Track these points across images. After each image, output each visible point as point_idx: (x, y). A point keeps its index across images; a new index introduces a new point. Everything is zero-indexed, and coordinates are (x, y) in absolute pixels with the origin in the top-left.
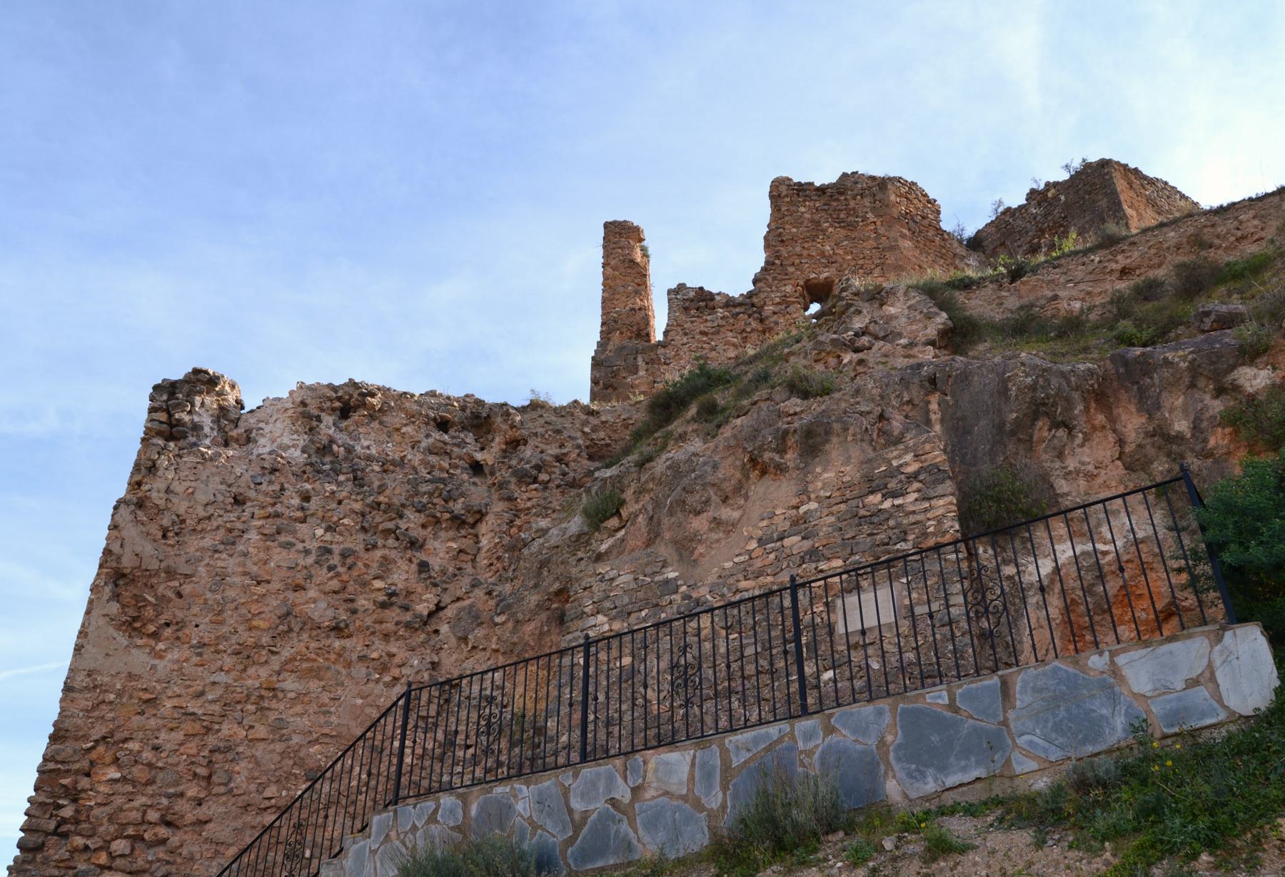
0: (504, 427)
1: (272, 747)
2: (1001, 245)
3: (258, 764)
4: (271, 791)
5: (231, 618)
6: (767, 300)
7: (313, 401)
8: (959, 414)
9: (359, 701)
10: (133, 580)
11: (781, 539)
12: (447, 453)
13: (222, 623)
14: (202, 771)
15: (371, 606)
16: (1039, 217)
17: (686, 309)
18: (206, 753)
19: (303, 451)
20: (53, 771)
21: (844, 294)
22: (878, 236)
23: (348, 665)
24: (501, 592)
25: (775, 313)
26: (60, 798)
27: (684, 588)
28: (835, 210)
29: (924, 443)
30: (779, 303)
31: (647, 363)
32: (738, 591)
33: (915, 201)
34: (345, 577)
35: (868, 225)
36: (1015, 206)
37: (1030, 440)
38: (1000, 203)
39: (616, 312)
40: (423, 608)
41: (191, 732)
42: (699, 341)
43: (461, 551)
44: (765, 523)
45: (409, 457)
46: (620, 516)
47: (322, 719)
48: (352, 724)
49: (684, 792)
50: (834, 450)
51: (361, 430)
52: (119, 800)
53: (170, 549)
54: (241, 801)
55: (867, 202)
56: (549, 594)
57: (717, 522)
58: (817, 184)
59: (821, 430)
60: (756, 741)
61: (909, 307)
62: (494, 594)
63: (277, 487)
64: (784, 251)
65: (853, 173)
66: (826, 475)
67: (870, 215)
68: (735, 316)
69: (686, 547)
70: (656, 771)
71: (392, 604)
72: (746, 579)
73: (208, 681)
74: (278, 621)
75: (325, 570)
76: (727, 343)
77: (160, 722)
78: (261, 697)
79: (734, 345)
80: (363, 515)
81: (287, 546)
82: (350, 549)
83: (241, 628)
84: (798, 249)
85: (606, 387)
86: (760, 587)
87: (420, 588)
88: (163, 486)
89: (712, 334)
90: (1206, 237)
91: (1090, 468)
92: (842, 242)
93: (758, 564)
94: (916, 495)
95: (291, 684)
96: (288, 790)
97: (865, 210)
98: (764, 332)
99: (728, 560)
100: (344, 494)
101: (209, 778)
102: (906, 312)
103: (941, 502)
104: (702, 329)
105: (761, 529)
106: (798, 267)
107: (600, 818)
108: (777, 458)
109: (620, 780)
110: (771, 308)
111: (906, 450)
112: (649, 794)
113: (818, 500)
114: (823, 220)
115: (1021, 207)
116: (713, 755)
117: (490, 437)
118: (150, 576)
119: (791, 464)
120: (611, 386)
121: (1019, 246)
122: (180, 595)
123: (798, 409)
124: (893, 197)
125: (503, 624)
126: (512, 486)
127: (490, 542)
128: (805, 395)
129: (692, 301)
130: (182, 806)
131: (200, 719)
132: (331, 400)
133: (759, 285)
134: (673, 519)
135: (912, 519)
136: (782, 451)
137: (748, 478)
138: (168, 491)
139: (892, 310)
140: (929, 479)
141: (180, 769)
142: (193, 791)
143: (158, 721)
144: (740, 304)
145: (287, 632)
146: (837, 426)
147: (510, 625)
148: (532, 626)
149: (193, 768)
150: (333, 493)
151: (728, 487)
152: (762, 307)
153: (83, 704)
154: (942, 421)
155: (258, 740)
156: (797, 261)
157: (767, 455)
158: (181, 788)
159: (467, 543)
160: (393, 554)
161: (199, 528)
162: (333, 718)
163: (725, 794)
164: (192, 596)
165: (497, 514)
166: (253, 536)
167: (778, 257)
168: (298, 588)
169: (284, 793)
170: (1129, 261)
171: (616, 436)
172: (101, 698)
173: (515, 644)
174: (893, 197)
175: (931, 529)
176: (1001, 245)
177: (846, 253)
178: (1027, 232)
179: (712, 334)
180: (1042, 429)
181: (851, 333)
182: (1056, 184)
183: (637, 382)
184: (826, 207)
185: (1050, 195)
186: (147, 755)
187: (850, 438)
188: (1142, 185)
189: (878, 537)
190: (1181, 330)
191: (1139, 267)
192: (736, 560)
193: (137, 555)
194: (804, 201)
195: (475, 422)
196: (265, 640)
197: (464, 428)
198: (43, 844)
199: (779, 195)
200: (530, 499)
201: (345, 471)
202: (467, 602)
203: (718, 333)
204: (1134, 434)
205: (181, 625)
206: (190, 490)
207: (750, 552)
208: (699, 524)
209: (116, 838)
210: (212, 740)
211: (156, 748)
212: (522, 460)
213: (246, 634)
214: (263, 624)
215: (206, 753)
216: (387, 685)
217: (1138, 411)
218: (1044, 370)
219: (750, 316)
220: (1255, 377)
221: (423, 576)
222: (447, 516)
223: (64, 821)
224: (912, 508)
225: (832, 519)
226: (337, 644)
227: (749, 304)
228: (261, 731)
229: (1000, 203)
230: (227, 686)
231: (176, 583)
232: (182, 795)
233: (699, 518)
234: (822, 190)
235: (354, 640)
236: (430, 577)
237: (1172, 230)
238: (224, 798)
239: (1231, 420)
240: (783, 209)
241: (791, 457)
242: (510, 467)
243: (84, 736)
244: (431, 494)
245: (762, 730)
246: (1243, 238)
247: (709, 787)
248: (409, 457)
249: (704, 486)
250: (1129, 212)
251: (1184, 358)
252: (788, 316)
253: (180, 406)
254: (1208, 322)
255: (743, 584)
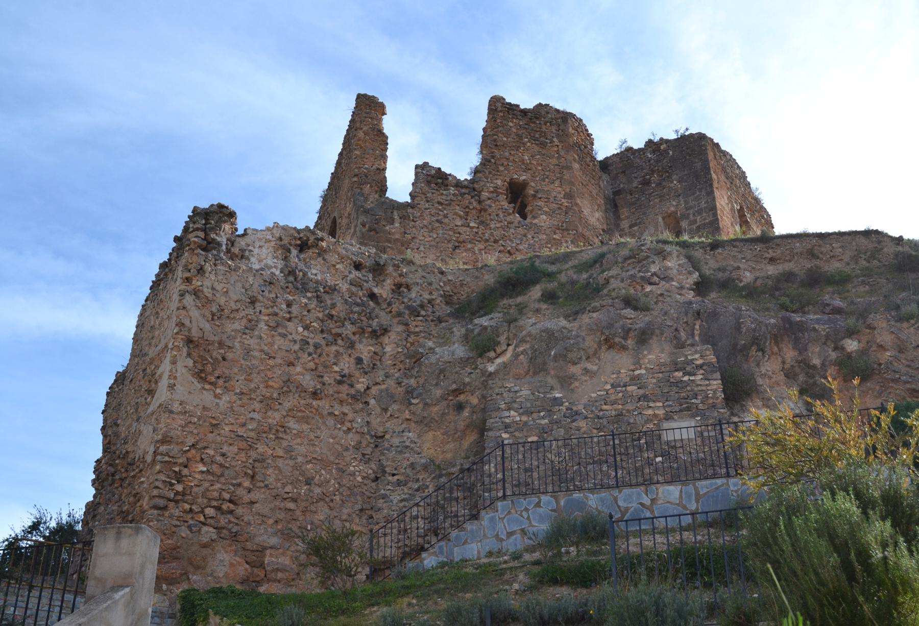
0: (395, 274)
1: (286, 462)
2: (622, 172)
3: (280, 471)
4: (288, 488)
5: (257, 378)
6: (485, 188)
7: (286, 238)
8: (710, 334)
9: (331, 440)
10: (197, 345)
11: (625, 386)
12: (360, 286)
13: (251, 381)
14: (250, 472)
15: (332, 381)
16: (652, 161)
17: (429, 183)
18: (251, 461)
19: (281, 272)
20: (166, 462)
21: (643, 248)
22: (560, 157)
23: (322, 417)
24: (407, 384)
25: (489, 199)
26: (172, 479)
27: (567, 404)
28: (532, 130)
29: (706, 350)
30: (492, 192)
31: (400, 218)
32: (601, 410)
33: (582, 134)
34: (317, 361)
35: (553, 146)
36: (636, 147)
37: (748, 356)
38: (625, 142)
39: (366, 168)
40: (360, 387)
41: (242, 447)
42: (437, 209)
43: (375, 353)
44: (615, 376)
45: (340, 285)
46: (495, 351)
47: (312, 449)
48: (328, 453)
49: (678, 502)
50: (654, 342)
51: (312, 262)
52: (206, 484)
53: (217, 328)
54: (274, 492)
55: (554, 129)
56: (448, 391)
57: (586, 371)
58: (522, 107)
59: (649, 332)
60: (711, 485)
61: (679, 265)
62: (403, 384)
63: (274, 296)
64: (497, 154)
65: (546, 105)
66: (650, 357)
67: (555, 139)
68: (462, 195)
69: (566, 381)
70: (663, 493)
71: (344, 382)
72: (605, 404)
73: (248, 417)
74: (283, 384)
75: (306, 355)
76: (456, 214)
77: (224, 439)
78: (277, 431)
79: (460, 216)
80: (322, 321)
81: (284, 336)
82: (319, 344)
83: (261, 386)
84: (507, 154)
85: (370, 230)
86: (615, 410)
87: (357, 374)
88: (209, 284)
89: (446, 205)
90: (816, 252)
91: (770, 373)
92: (536, 155)
93: (613, 397)
94: (701, 377)
95: (292, 424)
96: (297, 489)
97: (552, 135)
98: (480, 211)
99: (593, 393)
100: (313, 306)
101: (253, 477)
102: (677, 267)
103: (715, 382)
104: (439, 200)
105: (613, 379)
106: (507, 167)
107: (635, 510)
108: (623, 342)
109: (644, 496)
110: (487, 194)
111: (696, 352)
112: (660, 502)
113: (646, 369)
114: (524, 135)
115: (640, 150)
116: (690, 488)
117: (382, 278)
118: (209, 344)
119: (630, 347)
120: (374, 230)
121: (635, 178)
122: (224, 359)
123: (633, 316)
124: (570, 130)
125: (418, 404)
126: (406, 316)
127: (393, 350)
128: (635, 309)
129: (433, 177)
130: (241, 492)
131: (246, 440)
132: (295, 238)
133: (479, 175)
134: (556, 364)
135: (700, 388)
136: (625, 338)
137: (600, 348)
138: (213, 289)
139: (669, 264)
140: (709, 369)
141: (237, 469)
142: (247, 484)
143: (223, 438)
144: (466, 187)
145: (288, 392)
146: (657, 332)
147: (421, 405)
148: (436, 409)
149: (244, 469)
150: (306, 305)
151: (591, 351)
152: (480, 192)
153: (180, 422)
154: (700, 335)
155: (278, 457)
156: (506, 163)
157: (617, 340)
158: (239, 481)
159: (378, 349)
160: (341, 350)
161: (232, 316)
162: (318, 449)
163: (697, 505)
164: (232, 361)
165: (398, 333)
166: (262, 325)
167: (493, 157)
168: (291, 364)
169: (295, 491)
170: (775, 254)
171: (455, 291)
172: (189, 419)
173: (424, 417)
174: (570, 130)
175: (710, 395)
176: (622, 172)
177: (538, 164)
178: (642, 169)
179: (446, 205)
180: (753, 351)
181: (650, 274)
182: (667, 141)
183: (393, 231)
184: (527, 126)
185: (662, 147)
186: (219, 459)
187: (663, 339)
188: (720, 156)
189: (682, 394)
190: (811, 307)
191: (780, 259)
192: (599, 393)
193: (201, 329)
194: (513, 118)
195: (376, 267)
196: (275, 395)
197: (370, 271)
198: (167, 506)
199: (496, 110)
200: (416, 326)
201: (311, 290)
202: (383, 387)
203: (449, 205)
204: (790, 360)
205: (227, 379)
206: (225, 290)
207: (607, 391)
208: (575, 370)
209: (207, 507)
210: (253, 454)
211: (223, 455)
212: (411, 299)
213: (265, 390)
214: (276, 386)
215: (251, 461)
216: (345, 432)
217: (793, 348)
218: (760, 322)
219: (472, 197)
220: (851, 345)
221: (359, 366)
222: (370, 329)
223: (177, 493)
224: (699, 383)
225: (655, 381)
226: (314, 403)
227: (469, 188)
228: (280, 452)
229: (625, 142)
230: (259, 421)
231: (222, 351)
232: (239, 485)
233: (575, 367)
234: (525, 112)
235: (323, 401)
236: (363, 368)
237: (798, 242)
238: (263, 490)
239: (840, 364)
240: (498, 121)
241: (630, 343)
242: (403, 303)
243: (182, 442)
244: (359, 314)
245: (713, 481)
246: (833, 257)
247: (690, 501)
248: (340, 285)
249: (579, 349)
250: (714, 176)
251: (824, 330)
252: (497, 203)
253: (212, 229)
254: (828, 309)
255: (605, 407)
